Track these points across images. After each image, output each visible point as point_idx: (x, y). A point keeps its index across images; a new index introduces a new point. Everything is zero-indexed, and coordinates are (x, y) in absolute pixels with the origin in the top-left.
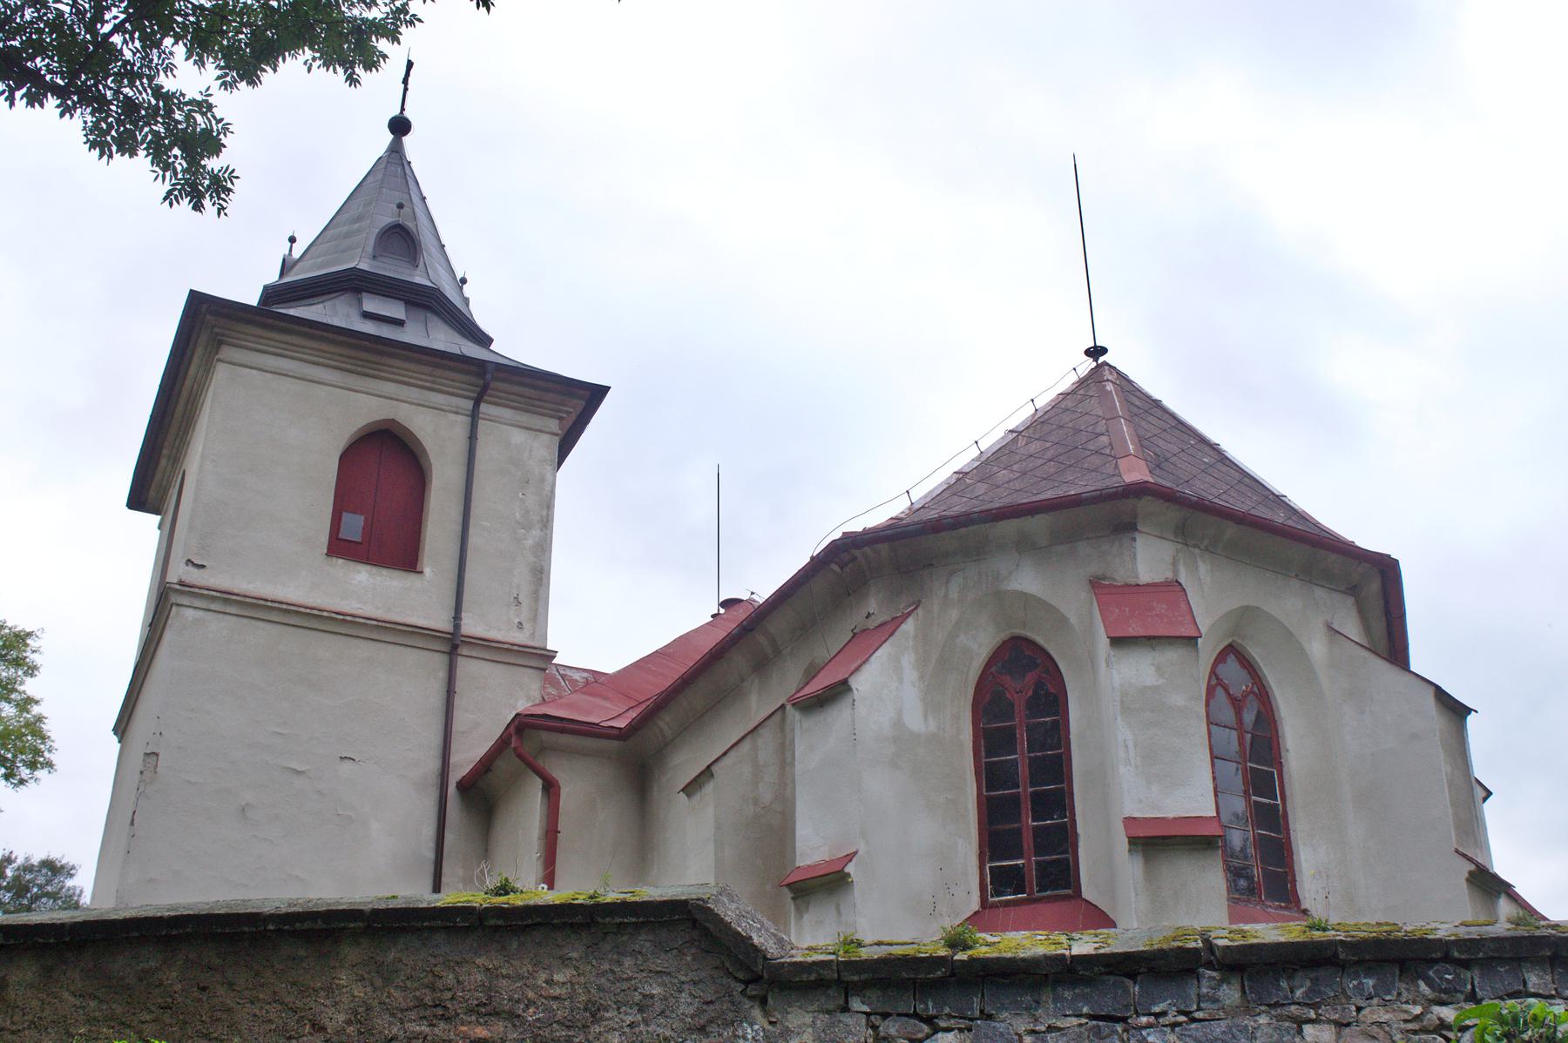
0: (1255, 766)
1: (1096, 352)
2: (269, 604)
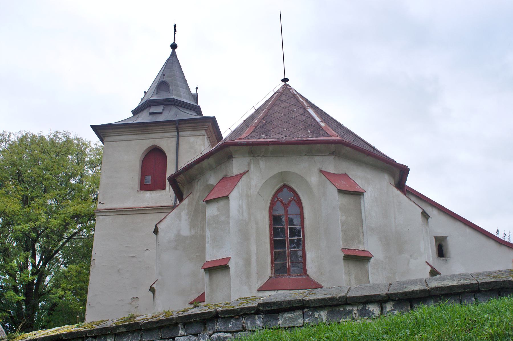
0: (291, 226)
1: (285, 80)
2: (121, 210)
